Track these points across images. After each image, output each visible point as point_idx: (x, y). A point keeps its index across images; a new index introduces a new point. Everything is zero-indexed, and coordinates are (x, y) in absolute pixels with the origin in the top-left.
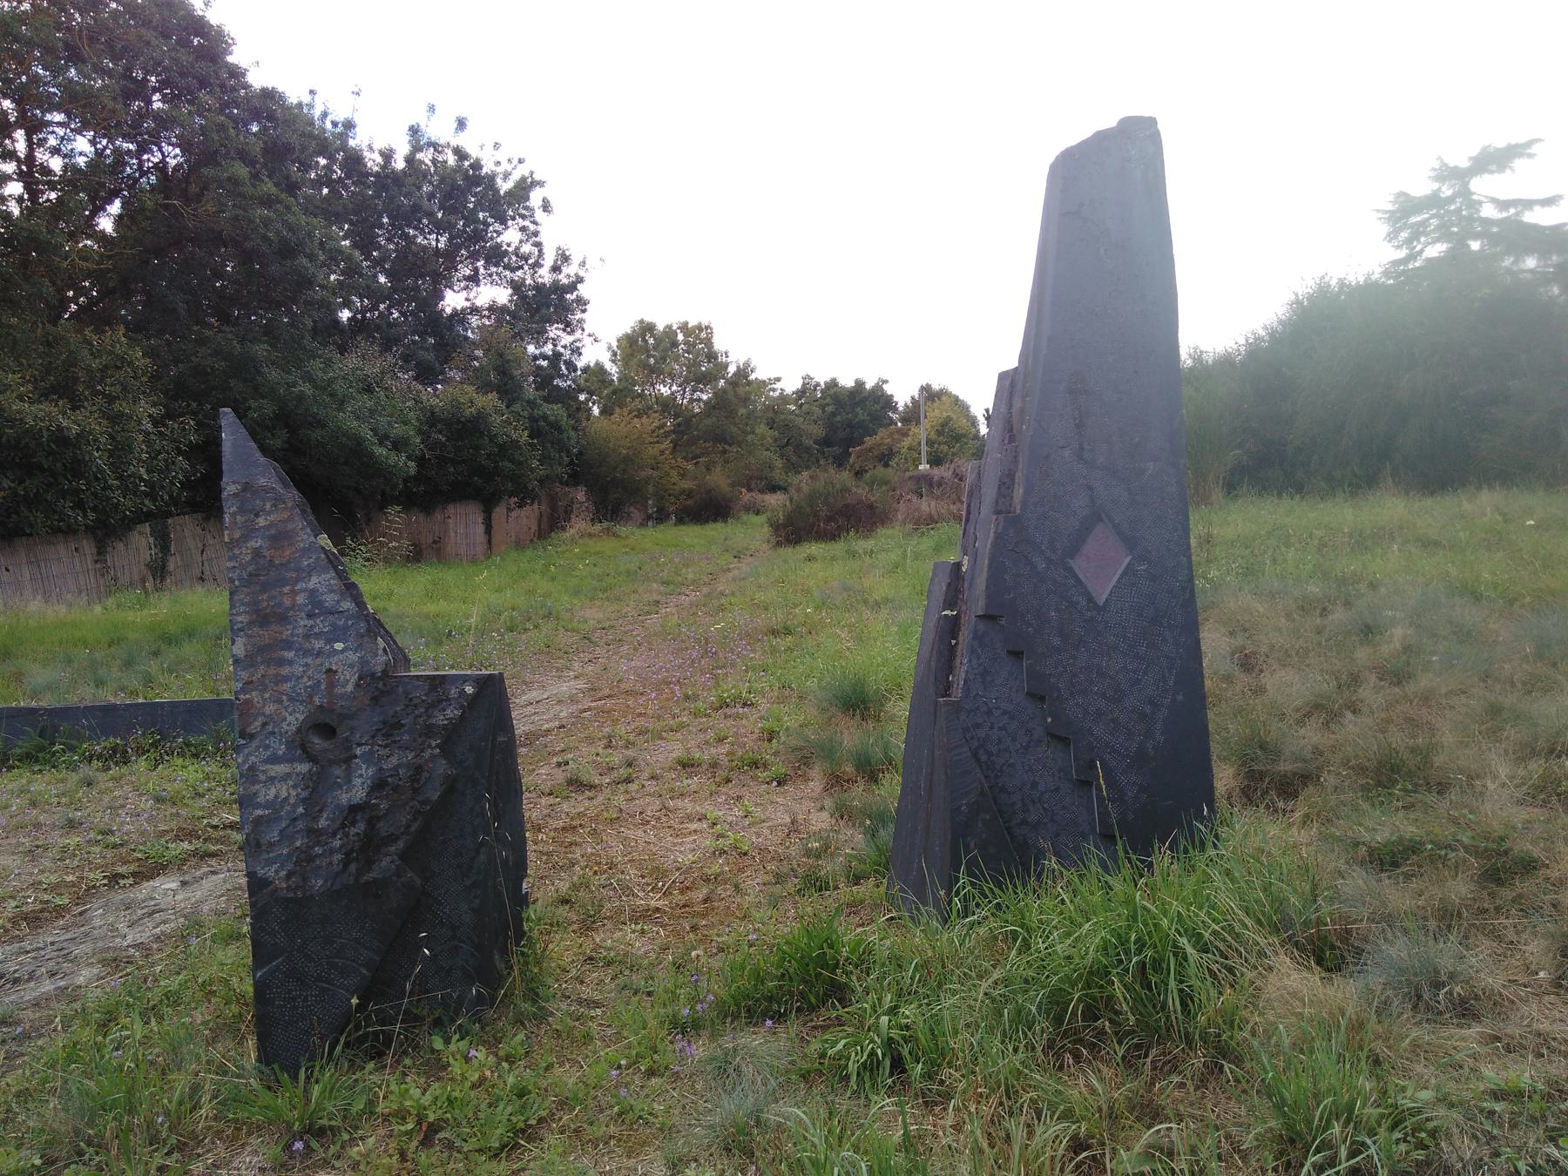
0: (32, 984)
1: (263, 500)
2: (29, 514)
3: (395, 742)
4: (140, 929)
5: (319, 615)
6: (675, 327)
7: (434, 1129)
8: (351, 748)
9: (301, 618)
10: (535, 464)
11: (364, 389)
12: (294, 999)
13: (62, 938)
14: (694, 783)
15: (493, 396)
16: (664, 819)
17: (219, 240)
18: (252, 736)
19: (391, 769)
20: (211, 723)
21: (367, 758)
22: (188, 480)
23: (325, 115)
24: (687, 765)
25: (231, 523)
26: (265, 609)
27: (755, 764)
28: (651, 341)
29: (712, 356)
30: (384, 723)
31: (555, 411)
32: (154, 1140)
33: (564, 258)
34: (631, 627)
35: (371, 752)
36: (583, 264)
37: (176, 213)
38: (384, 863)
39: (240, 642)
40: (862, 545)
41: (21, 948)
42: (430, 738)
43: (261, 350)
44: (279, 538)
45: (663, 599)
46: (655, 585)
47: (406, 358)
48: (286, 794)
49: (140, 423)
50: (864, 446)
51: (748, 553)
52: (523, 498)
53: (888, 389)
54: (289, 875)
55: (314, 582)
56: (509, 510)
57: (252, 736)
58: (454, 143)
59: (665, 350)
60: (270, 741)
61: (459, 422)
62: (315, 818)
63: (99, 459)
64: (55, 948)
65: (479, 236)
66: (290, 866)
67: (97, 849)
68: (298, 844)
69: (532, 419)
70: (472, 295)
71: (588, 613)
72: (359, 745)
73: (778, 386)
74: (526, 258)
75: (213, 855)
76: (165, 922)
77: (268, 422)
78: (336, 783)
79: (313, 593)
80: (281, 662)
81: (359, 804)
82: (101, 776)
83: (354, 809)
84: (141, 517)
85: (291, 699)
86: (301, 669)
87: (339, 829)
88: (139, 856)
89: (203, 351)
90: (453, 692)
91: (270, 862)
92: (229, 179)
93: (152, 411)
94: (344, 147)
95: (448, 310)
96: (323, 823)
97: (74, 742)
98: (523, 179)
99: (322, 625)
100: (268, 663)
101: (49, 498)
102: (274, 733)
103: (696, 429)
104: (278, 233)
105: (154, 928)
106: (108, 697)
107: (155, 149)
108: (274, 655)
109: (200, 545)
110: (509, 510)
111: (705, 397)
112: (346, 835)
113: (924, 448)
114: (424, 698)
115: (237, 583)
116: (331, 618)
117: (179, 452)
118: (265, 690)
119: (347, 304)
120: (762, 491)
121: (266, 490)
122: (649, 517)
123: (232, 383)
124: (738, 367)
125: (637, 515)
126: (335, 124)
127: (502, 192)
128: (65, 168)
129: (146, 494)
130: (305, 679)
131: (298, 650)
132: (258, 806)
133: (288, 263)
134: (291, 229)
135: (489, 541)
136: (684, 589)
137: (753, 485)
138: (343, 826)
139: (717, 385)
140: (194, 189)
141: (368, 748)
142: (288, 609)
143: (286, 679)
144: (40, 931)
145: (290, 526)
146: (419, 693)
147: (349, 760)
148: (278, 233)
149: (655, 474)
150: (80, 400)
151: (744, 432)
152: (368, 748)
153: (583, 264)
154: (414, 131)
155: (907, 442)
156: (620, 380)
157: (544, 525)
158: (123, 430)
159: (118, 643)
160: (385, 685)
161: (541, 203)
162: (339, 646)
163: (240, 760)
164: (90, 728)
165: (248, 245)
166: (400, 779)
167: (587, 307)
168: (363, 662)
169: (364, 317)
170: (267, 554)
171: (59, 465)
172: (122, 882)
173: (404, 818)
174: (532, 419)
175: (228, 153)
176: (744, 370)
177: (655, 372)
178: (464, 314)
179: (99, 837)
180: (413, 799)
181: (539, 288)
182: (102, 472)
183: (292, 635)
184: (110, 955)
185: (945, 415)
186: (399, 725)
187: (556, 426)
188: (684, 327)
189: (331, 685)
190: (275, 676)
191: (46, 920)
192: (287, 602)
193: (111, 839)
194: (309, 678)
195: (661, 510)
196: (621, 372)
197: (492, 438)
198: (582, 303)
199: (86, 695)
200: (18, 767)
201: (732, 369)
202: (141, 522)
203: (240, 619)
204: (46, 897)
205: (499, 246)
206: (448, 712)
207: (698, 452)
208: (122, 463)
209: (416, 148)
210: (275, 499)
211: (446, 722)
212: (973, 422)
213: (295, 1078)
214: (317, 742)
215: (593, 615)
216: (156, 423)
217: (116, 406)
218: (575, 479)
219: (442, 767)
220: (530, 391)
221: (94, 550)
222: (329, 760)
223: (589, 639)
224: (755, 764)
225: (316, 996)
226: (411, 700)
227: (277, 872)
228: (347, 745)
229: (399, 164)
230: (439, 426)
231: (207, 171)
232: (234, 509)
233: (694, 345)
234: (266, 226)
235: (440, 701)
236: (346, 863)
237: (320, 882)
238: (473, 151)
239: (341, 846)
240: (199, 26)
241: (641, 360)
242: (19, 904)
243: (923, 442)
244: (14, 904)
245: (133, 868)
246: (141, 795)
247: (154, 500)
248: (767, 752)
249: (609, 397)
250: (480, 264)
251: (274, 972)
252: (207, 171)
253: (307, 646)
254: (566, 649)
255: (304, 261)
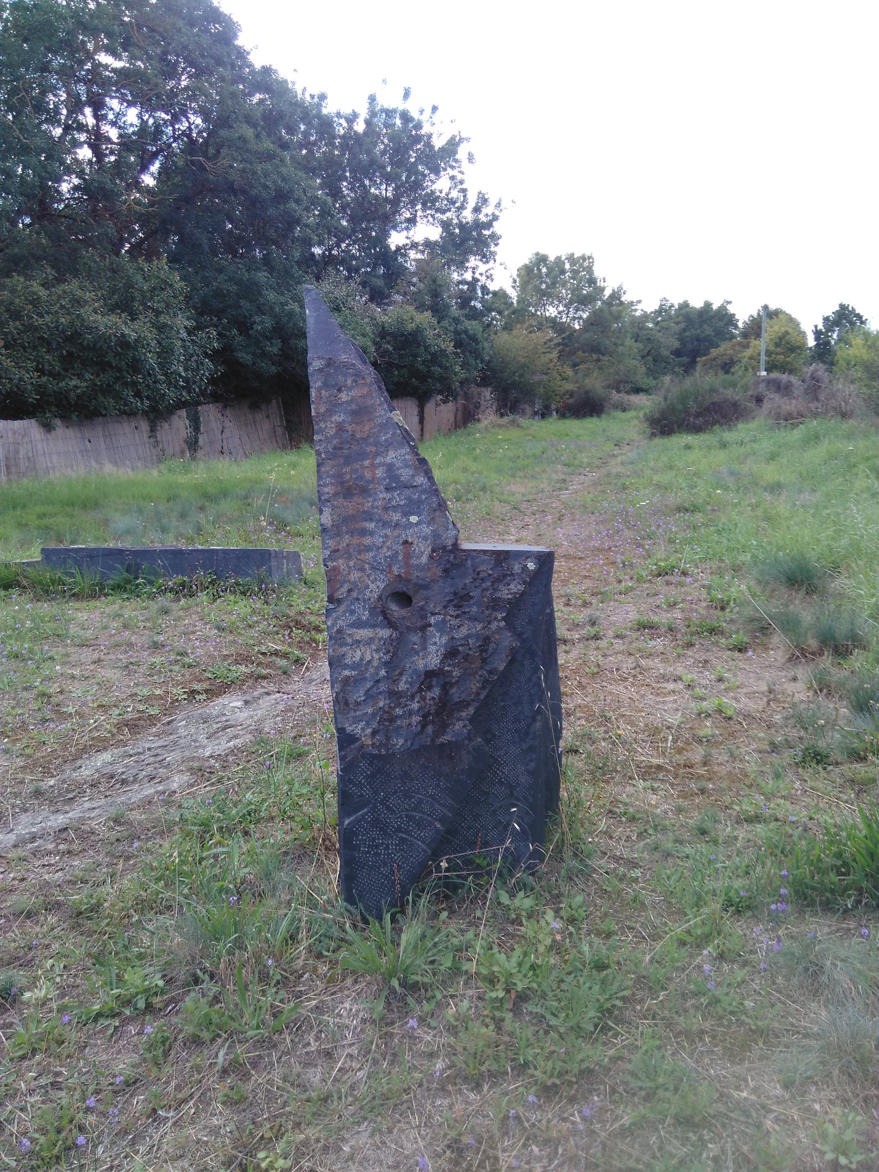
0: (136, 787)
1: (345, 376)
2: (104, 400)
3: (464, 613)
4: (217, 742)
5: (395, 489)
6: (563, 258)
7: (523, 997)
8: (425, 617)
9: (381, 492)
10: (457, 369)
11: (334, 309)
12: (377, 847)
13: (156, 745)
14: (658, 644)
15: (428, 314)
16: (640, 677)
17: (231, 189)
18: (339, 601)
19: (462, 639)
20: (254, 568)
21: (441, 627)
22: (213, 378)
23: (304, 90)
24: (645, 627)
25: (317, 397)
26: (349, 481)
27: (713, 631)
28: (544, 270)
29: (592, 281)
30: (455, 594)
31: (472, 326)
32: (264, 977)
33: (483, 200)
34: (549, 501)
35: (444, 621)
36: (498, 205)
37: (202, 168)
38: (457, 727)
39: (327, 512)
40: (729, 436)
41: (125, 752)
42: (496, 610)
43: (262, 276)
44: (360, 413)
45: (568, 478)
46: (559, 467)
47: (364, 284)
48: (370, 658)
49: (178, 332)
50: (709, 357)
51: (626, 442)
52: (447, 396)
53: (731, 309)
54: (374, 733)
55: (391, 456)
56: (437, 405)
57: (339, 601)
58: (401, 108)
59: (555, 277)
60: (356, 607)
61: (403, 335)
62: (395, 681)
63: (151, 359)
64: (152, 753)
65: (417, 186)
66: (375, 725)
67: (176, 668)
68: (381, 704)
69: (457, 333)
70: (411, 233)
71: (513, 488)
72: (433, 614)
73: (639, 307)
74: (452, 202)
75: (264, 677)
76: (236, 737)
77: (268, 334)
78: (413, 649)
79: (390, 467)
80: (364, 532)
81: (434, 670)
82: (174, 606)
83: (430, 674)
84: (181, 404)
85: (373, 568)
86: (381, 540)
87: (416, 692)
88: (210, 676)
89: (222, 277)
90: (517, 568)
91: (357, 720)
92: (240, 138)
93: (186, 323)
94: (319, 116)
95: (393, 248)
96: (402, 686)
97: (152, 578)
98: (453, 138)
99: (399, 499)
100: (352, 533)
101: (117, 388)
102: (358, 599)
103: (577, 342)
104: (274, 182)
105: (228, 742)
106: (171, 543)
107: (184, 119)
108: (357, 526)
109: (220, 427)
110: (437, 405)
111: (585, 316)
112: (423, 699)
113: (763, 358)
114: (490, 572)
115: (323, 456)
116: (407, 492)
117: (206, 355)
118: (350, 558)
119: (320, 243)
120: (628, 393)
121: (348, 366)
122: (536, 413)
123: (242, 302)
124: (613, 290)
125: (529, 410)
126: (312, 97)
127: (436, 148)
128: (121, 136)
129: (183, 387)
130: (385, 550)
131: (378, 522)
132: (346, 667)
133: (282, 207)
134: (284, 180)
135: (422, 430)
136: (581, 470)
137: (621, 388)
138: (420, 690)
139: (594, 307)
140: (212, 151)
141: (440, 617)
142: (368, 482)
143: (368, 549)
144: (138, 736)
145: (369, 402)
146: (486, 568)
147: (424, 628)
148: (274, 182)
149: (545, 377)
150: (136, 314)
151: (615, 344)
152: (440, 617)
153: (498, 205)
154: (372, 99)
155: (748, 353)
156: (518, 302)
157: (459, 418)
158: (167, 338)
159: (174, 500)
160: (455, 558)
161: (467, 156)
162: (414, 519)
163: (329, 623)
164: (164, 567)
165: (253, 192)
166: (470, 649)
167: (499, 241)
168: (436, 535)
169: (330, 253)
170: (349, 428)
171: (123, 363)
172: (198, 697)
173: (474, 685)
174: (457, 333)
175: (237, 117)
176: (618, 293)
177: (547, 295)
178: (405, 250)
179: (179, 658)
180: (482, 668)
181: (461, 226)
182: (153, 369)
183: (373, 507)
184: (196, 764)
185: (783, 330)
186: (467, 597)
187: (474, 339)
188: (571, 258)
189: (408, 556)
190: (359, 545)
191: (143, 727)
192: (368, 475)
193: (187, 660)
194: (388, 548)
195: (547, 407)
196: (518, 296)
197: (427, 348)
198: (495, 238)
199: (154, 541)
200: (112, 595)
201: (607, 293)
202: (180, 408)
203: (326, 490)
204: (142, 708)
205: (433, 192)
206: (512, 586)
207: (577, 360)
208: (167, 363)
209: (373, 113)
210: (355, 375)
211: (510, 596)
212: (803, 334)
213: (380, 918)
214: (394, 608)
215: (518, 489)
216: (189, 332)
217: (163, 319)
218: (485, 382)
219: (507, 640)
220: (454, 311)
221: (149, 429)
222: (408, 628)
223: (518, 509)
224: (713, 631)
225: (396, 845)
226: (478, 573)
227: (363, 729)
228: (423, 613)
229: (360, 127)
230: (388, 338)
231: (224, 133)
232: (319, 384)
233: (578, 272)
234: (265, 177)
235: (505, 576)
236: (424, 725)
237: (401, 741)
238: (415, 114)
239: (420, 708)
240: (216, 15)
241: (535, 286)
242: (121, 712)
243: (763, 353)
244: (117, 712)
245: (206, 685)
246: (206, 624)
247: (189, 392)
248: (721, 619)
249: (509, 316)
250: (419, 207)
251: (360, 821)
252: (224, 133)
253: (386, 517)
254: (502, 516)
255: (293, 205)
